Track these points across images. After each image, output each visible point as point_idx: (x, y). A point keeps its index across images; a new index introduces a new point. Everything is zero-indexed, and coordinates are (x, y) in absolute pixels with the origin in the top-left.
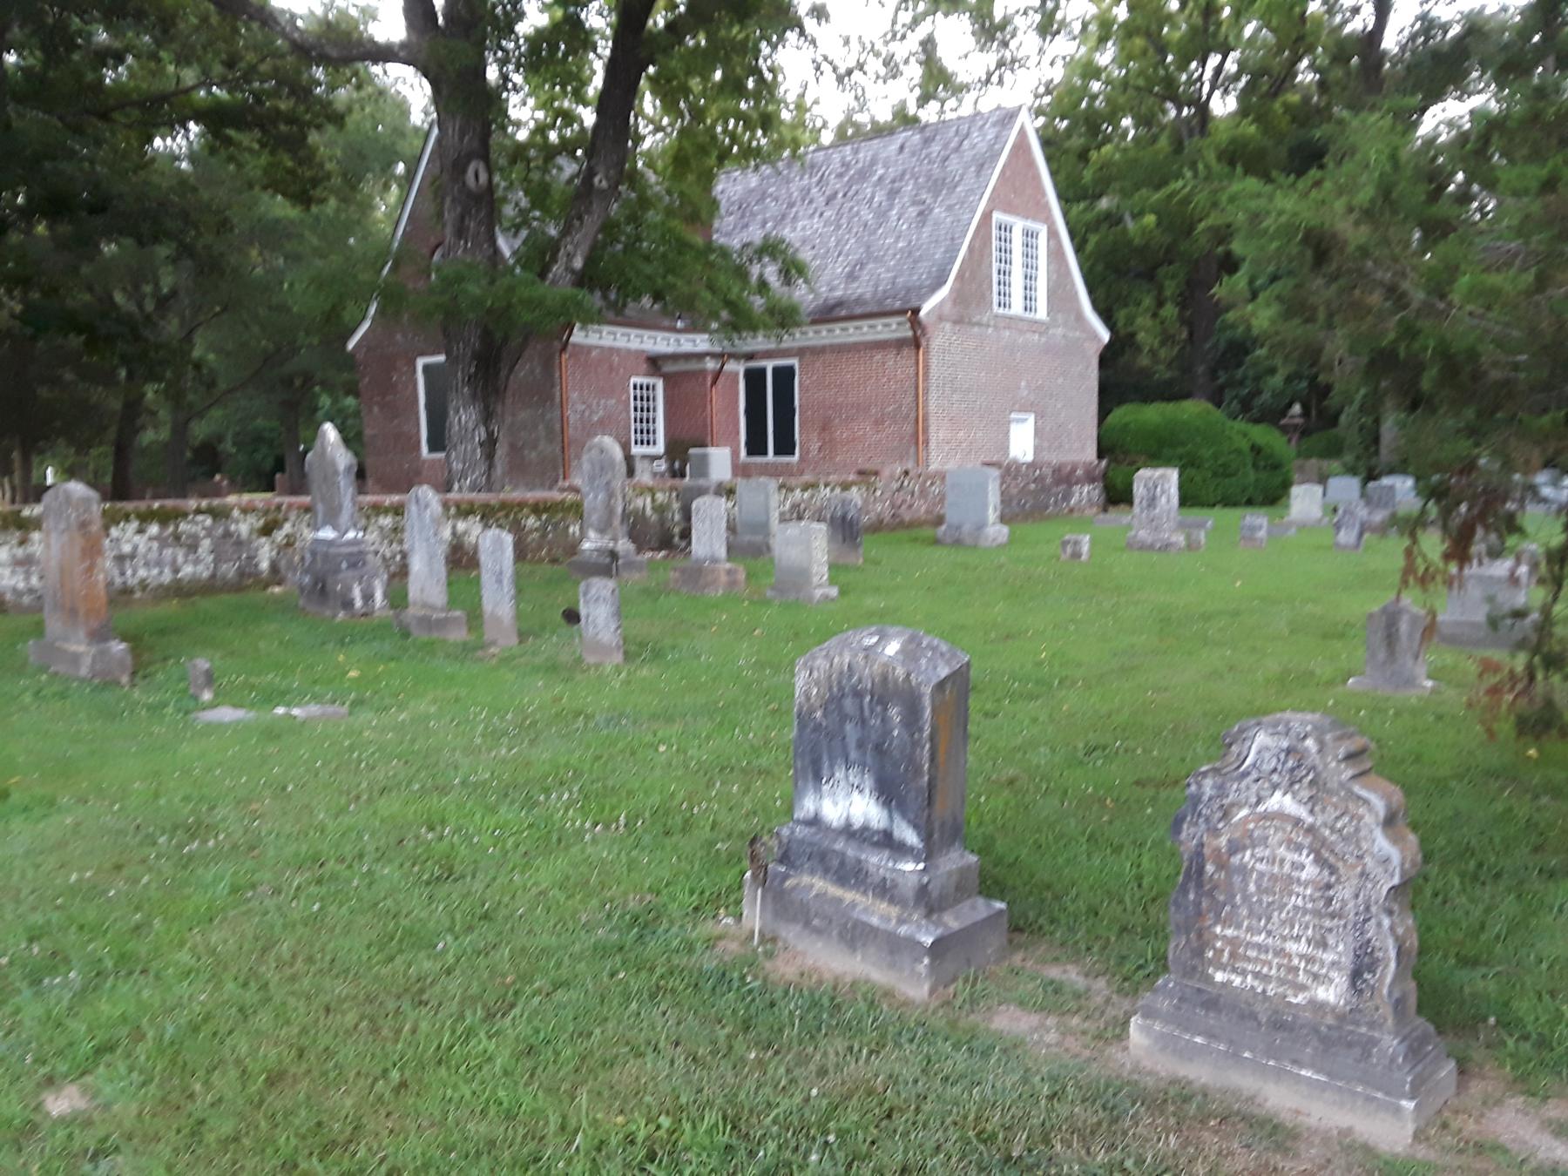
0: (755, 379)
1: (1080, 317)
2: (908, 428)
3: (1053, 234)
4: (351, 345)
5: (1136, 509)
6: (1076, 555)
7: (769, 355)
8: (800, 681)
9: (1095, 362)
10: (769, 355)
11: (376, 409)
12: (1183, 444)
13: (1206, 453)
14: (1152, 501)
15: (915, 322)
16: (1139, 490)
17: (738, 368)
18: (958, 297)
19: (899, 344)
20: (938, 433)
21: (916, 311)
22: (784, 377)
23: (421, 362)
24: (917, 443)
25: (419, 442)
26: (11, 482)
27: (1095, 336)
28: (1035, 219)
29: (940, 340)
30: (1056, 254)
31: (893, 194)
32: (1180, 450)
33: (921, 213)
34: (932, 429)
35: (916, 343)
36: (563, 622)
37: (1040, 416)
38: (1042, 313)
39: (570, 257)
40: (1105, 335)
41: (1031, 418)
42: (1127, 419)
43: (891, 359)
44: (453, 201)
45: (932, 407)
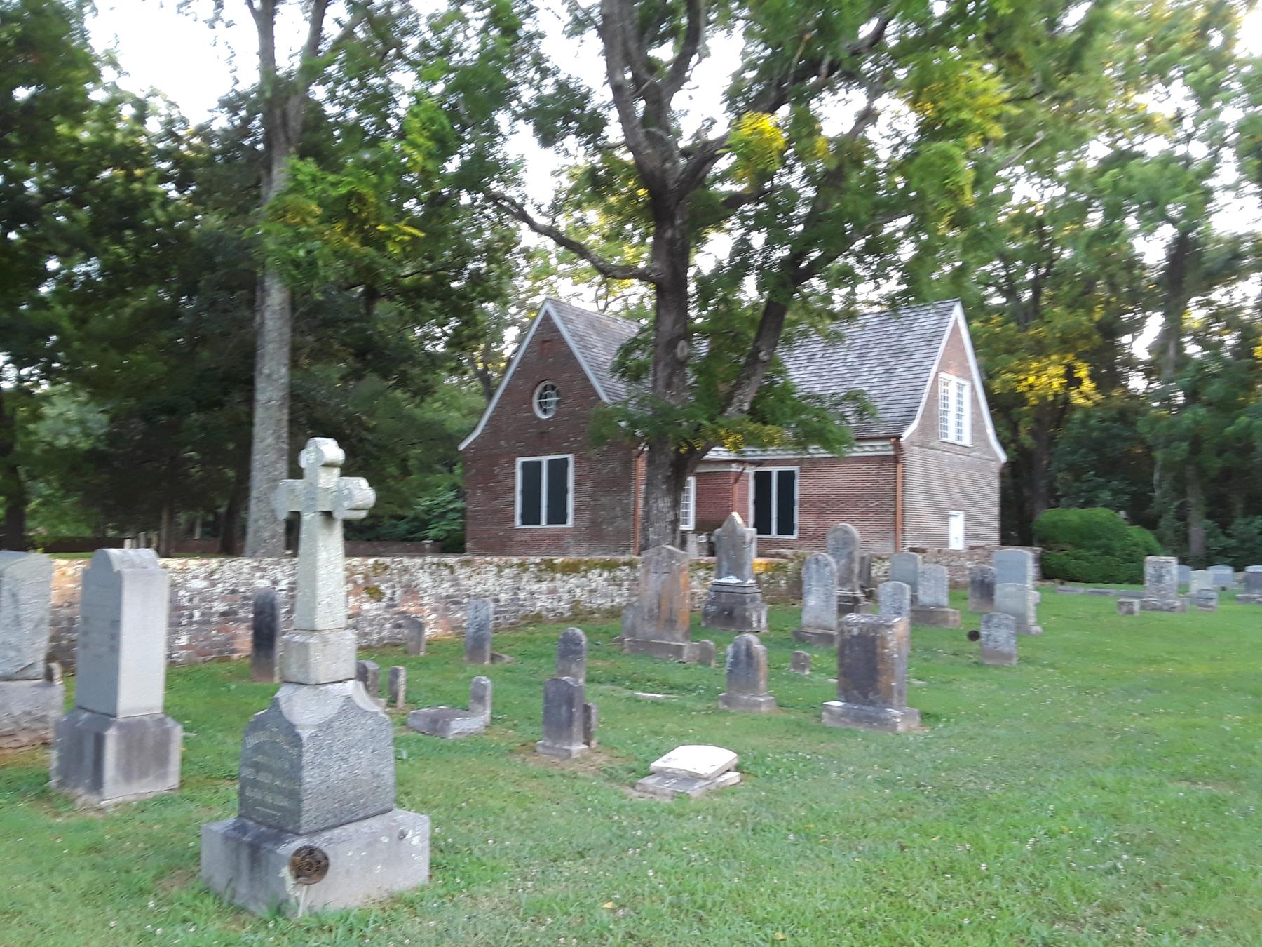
0: (762, 481)
1: (988, 445)
2: (889, 518)
3: (973, 388)
4: (462, 447)
5: (1147, 584)
6: (1131, 612)
7: (774, 463)
8: (895, 712)
9: (997, 475)
10: (774, 463)
11: (479, 493)
12: (1098, 537)
13: (1117, 544)
14: (1159, 578)
15: (897, 446)
16: (1149, 570)
17: (751, 471)
18: (923, 429)
19: (882, 459)
20: (911, 523)
21: (899, 437)
22: (787, 480)
23: (520, 461)
24: (895, 530)
25: (513, 517)
26: (159, 536)
27: (997, 459)
28: (964, 378)
29: (912, 456)
30: (975, 401)
31: (862, 356)
32: (1098, 542)
33: (887, 371)
34: (907, 519)
35: (895, 460)
36: (965, 637)
37: (968, 513)
38: (966, 440)
39: (742, 402)
40: (1003, 458)
41: (961, 515)
42: (1056, 518)
43: (874, 470)
44: (666, 365)
45: (907, 506)
